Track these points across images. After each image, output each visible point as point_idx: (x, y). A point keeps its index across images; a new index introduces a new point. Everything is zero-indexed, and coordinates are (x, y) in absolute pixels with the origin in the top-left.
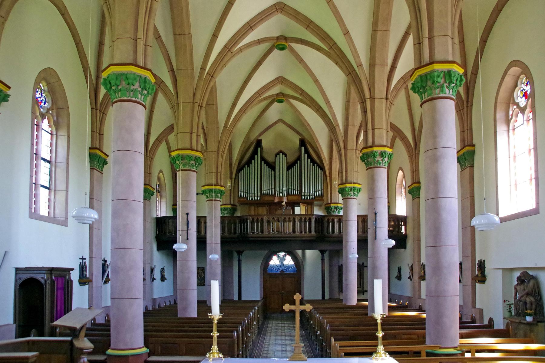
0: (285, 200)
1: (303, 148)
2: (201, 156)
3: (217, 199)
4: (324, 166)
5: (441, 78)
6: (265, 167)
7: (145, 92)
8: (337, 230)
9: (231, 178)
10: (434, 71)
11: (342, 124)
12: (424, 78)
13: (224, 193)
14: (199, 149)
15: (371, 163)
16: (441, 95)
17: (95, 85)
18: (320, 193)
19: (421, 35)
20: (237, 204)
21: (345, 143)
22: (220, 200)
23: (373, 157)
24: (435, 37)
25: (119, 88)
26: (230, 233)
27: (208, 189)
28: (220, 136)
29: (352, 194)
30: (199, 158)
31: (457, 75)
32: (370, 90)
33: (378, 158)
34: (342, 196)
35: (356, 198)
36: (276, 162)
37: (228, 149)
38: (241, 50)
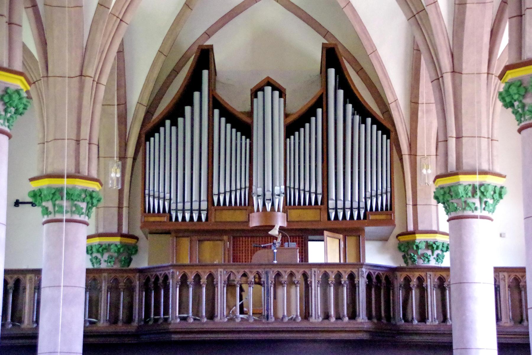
0: (280, 221)
1: (332, 72)
3: (76, 217)
4: (394, 125)
9: (122, 158)
13: (99, 201)
14: (18, 66)
20: (139, 233)
22: (86, 219)
26: (114, 320)
27: (49, 188)
34: (448, 212)
37: (113, 68)
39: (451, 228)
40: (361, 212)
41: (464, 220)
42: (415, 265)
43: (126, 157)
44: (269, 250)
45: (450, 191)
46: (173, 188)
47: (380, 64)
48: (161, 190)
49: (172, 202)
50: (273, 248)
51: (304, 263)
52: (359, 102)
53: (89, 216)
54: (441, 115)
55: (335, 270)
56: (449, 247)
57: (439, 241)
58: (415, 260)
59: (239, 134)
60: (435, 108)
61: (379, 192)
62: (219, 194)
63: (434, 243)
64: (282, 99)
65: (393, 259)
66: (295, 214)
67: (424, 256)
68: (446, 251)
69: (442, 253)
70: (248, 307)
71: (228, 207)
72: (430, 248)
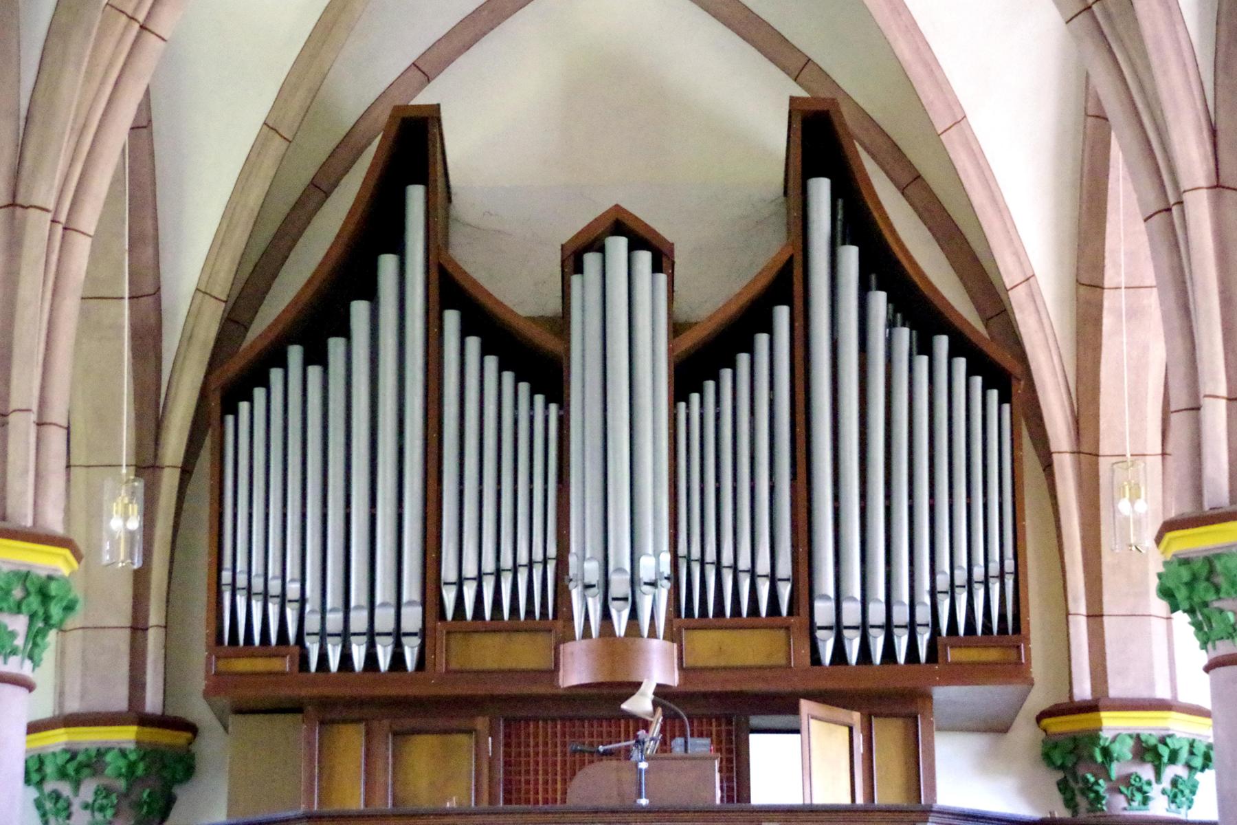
1: (821, 189)
4: (1022, 357)
9: (147, 467)
13: (69, 608)
20: (199, 710)
22: (26, 669)
37: (116, 181)
39: (1216, 695)
40: (919, 638)
42: (1099, 814)
43: (157, 464)
44: (623, 764)
45: (1212, 571)
46: (257, 560)
47: (983, 172)
48: (257, 569)
49: (308, 608)
50: (636, 755)
51: (736, 806)
52: (886, 248)
53: (36, 658)
54: (1177, 322)
56: (1213, 754)
57: (1178, 735)
58: (1099, 798)
59: (524, 387)
60: (1158, 302)
61: (978, 573)
62: (460, 583)
63: (1163, 741)
64: (662, 278)
65: (1026, 791)
67: (1128, 785)
68: (1203, 770)
69: (1189, 777)
71: (785, 618)
72: (1148, 757)
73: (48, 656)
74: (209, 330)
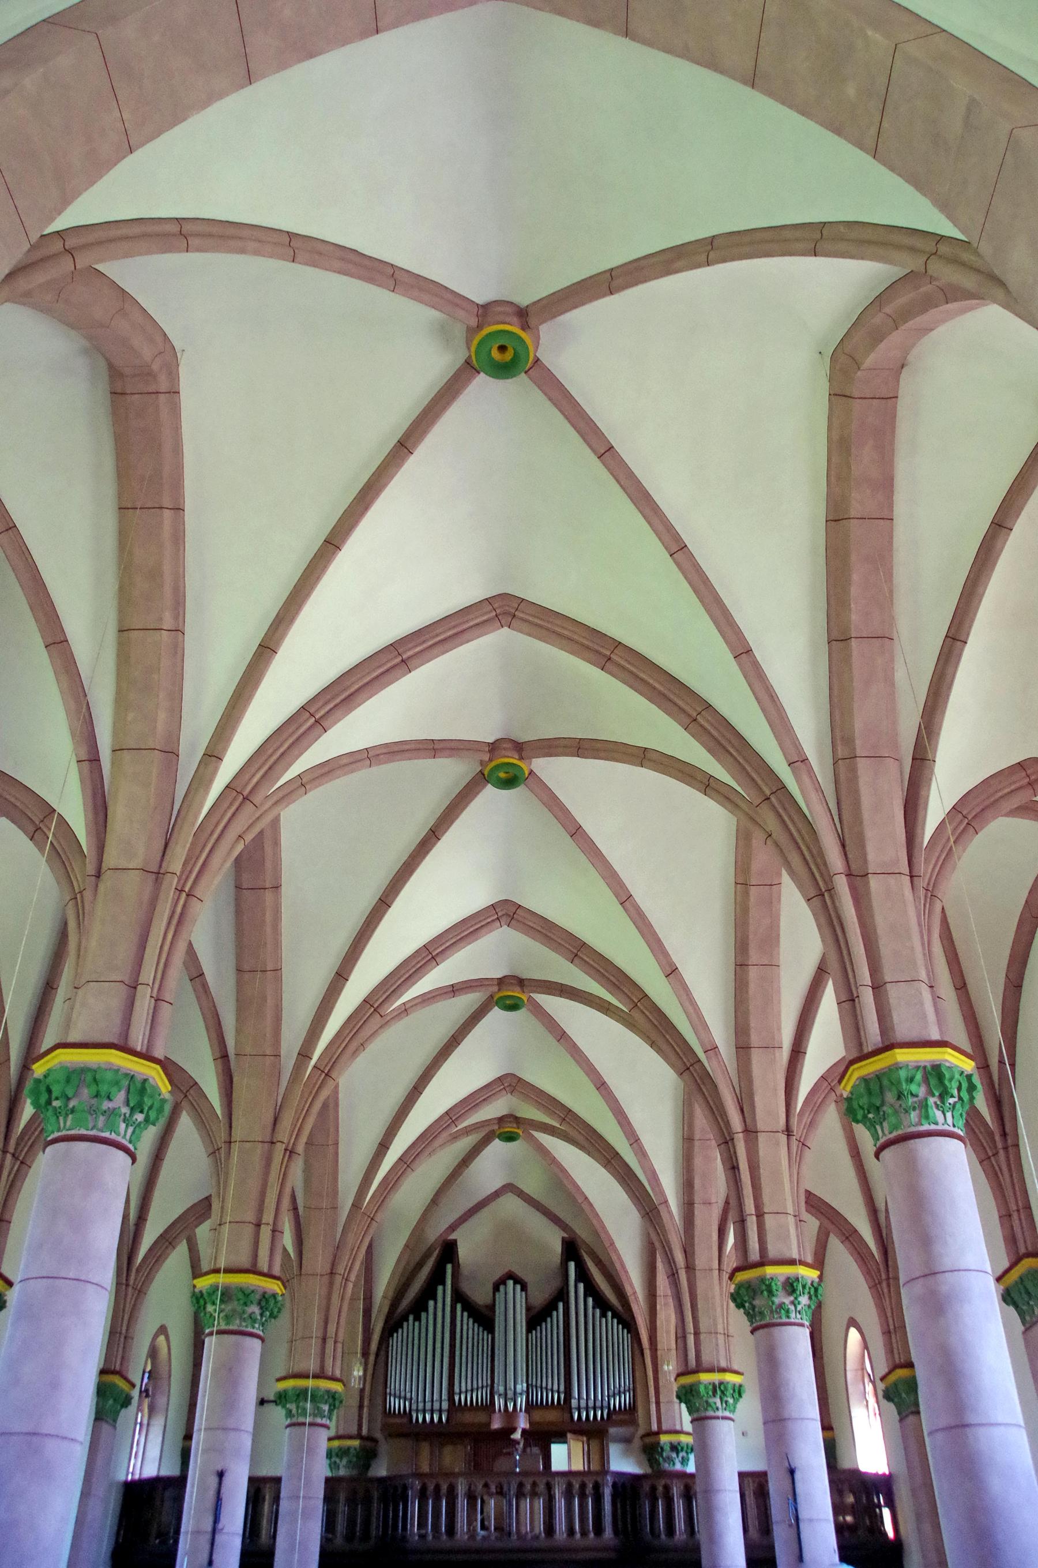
0: (523, 1423)
1: (572, 1265)
2: (279, 1291)
3: (319, 1420)
4: (633, 1318)
5: (919, 1085)
6: (465, 1321)
7: (140, 1117)
8: (680, 1524)
9: (365, 1354)
10: (897, 1067)
11: (677, 1197)
12: (875, 1087)
14: (277, 1270)
15: (761, 1313)
16: (926, 1127)
17: (13, 1087)
18: (626, 1399)
19: (852, 980)
20: (378, 1435)
21: (688, 1252)
22: (328, 1422)
23: (765, 1293)
24: (888, 985)
25: (71, 1104)
26: (349, 1537)
27: (294, 1388)
28: (340, 1229)
29: (719, 1404)
30: (274, 1295)
31: (957, 1076)
32: (742, 1110)
33: (781, 1298)
34: (690, 1412)
35: (731, 1415)
36: (497, 1307)
38: (405, 1010)
39: (693, 1428)
41: (784, 1328)
45: (691, 1390)
55: (579, 1479)
59: (481, 1329)
64: (524, 1293)
65: (639, 1464)
66: (538, 1416)
70: (490, 1521)
73: (334, 1418)
74: (386, 1310)
